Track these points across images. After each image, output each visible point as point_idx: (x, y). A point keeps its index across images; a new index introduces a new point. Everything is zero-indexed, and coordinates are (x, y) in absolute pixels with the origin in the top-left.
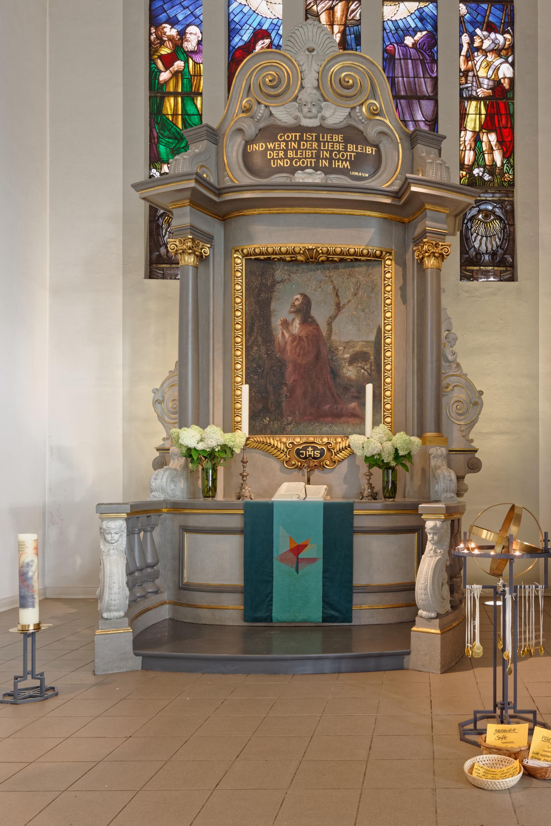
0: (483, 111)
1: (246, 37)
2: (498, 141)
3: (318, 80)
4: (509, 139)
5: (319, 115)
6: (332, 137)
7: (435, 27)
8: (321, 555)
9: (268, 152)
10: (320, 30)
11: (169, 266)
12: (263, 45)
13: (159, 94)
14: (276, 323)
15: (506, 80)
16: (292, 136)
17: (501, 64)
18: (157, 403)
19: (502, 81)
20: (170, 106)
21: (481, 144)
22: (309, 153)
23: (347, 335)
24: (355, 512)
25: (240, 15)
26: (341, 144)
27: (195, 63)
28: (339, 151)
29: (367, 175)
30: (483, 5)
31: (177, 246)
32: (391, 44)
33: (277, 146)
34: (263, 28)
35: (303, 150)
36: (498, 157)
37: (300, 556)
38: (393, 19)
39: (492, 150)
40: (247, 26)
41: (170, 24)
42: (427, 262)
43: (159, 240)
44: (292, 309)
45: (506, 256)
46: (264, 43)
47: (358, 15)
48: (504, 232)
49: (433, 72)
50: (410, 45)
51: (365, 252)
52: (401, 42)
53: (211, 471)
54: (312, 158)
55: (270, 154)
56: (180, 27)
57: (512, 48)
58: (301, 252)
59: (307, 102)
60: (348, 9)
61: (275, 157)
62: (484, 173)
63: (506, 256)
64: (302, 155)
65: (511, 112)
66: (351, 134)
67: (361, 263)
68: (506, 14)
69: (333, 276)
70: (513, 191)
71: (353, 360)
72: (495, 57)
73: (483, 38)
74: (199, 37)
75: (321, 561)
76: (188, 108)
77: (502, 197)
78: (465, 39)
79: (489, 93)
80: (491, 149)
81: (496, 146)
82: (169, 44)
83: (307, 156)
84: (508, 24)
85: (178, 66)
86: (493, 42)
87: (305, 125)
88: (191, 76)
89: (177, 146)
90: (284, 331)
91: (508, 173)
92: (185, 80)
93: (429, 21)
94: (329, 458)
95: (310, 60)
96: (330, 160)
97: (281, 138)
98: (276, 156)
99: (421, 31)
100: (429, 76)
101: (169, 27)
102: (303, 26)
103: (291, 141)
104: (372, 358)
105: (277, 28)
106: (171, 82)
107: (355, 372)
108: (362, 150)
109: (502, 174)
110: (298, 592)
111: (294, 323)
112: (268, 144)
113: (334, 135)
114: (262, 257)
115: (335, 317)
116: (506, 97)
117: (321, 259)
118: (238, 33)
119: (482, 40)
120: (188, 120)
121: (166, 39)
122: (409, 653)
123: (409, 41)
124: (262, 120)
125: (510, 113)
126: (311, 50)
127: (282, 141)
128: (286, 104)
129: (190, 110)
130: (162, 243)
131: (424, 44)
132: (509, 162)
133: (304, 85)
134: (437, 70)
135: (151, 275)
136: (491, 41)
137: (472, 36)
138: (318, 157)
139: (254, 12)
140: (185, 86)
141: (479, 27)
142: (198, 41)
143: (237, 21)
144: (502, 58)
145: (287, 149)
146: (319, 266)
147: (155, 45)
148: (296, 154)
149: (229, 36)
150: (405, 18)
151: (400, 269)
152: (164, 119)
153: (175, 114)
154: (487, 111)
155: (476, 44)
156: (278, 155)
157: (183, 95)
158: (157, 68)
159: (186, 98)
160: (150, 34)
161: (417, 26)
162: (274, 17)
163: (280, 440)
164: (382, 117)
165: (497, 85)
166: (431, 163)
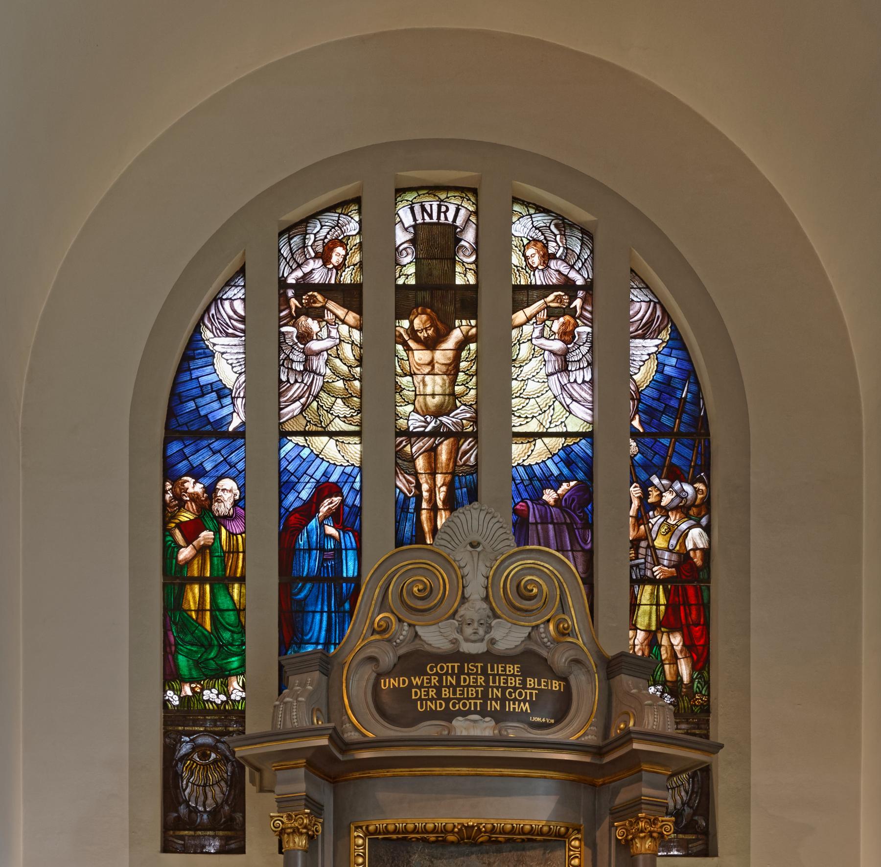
0: (663, 600)
3: (487, 588)
4: (702, 642)
5: (487, 637)
7: (590, 474)
9: (413, 690)
10: (489, 516)
11: (192, 833)
13: (178, 581)
15: (698, 553)
16: (448, 667)
17: (690, 528)
19: (692, 553)
20: (194, 597)
21: (660, 649)
22: (472, 692)
27: (230, 533)
28: (515, 688)
29: (552, 721)
31: (283, 823)
32: (523, 501)
34: (330, 480)
35: (463, 687)
36: (684, 669)
38: (526, 463)
39: (677, 658)
45: (696, 818)
46: (331, 503)
47: (472, 459)
48: (693, 781)
49: (585, 542)
50: (552, 502)
51: (546, 829)
52: (537, 498)
54: (477, 698)
55: (416, 692)
56: (207, 481)
57: (706, 505)
58: (456, 830)
59: (473, 620)
60: (458, 449)
62: (663, 693)
63: (696, 818)
64: (463, 694)
65: (705, 601)
66: (530, 661)
67: (535, 844)
68: (697, 452)
69: (494, 862)
70: (708, 720)
72: (681, 518)
73: (662, 489)
74: (235, 495)
77: (690, 729)
78: (635, 491)
79: (671, 572)
80: (674, 659)
81: (681, 652)
82: (192, 506)
84: (700, 468)
85: (205, 539)
86: (678, 495)
87: (466, 651)
88: (224, 552)
91: (701, 692)
93: (580, 465)
95: (476, 559)
96: (503, 700)
97: (431, 669)
99: (568, 481)
100: (580, 549)
101: (192, 480)
102: (466, 512)
103: (447, 674)
105: (351, 479)
106: (196, 562)
108: (547, 686)
109: (691, 695)
114: (394, 837)
117: (480, 840)
118: (293, 488)
119: (661, 493)
123: (549, 496)
126: (474, 545)
127: (433, 675)
128: (441, 621)
131: (573, 500)
132: (701, 676)
133: (467, 596)
135: (167, 848)
137: (645, 486)
138: (485, 697)
140: (216, 567)
142: (235, 501)
144: (691, 519)
145: (441, 686)
146: (474, 849)
147: (171, 507)
148: (455, 693)
149: (280, 493)
150: (543, 461)
151: (590, 852)
153: (200, 610)
156: (428, 695)
157: (212, 581)
158: (175, 541)
159: (217, 586)
160: (165, 492)
161: (561, 473)
164: (573, 637)
166: (650, 705)
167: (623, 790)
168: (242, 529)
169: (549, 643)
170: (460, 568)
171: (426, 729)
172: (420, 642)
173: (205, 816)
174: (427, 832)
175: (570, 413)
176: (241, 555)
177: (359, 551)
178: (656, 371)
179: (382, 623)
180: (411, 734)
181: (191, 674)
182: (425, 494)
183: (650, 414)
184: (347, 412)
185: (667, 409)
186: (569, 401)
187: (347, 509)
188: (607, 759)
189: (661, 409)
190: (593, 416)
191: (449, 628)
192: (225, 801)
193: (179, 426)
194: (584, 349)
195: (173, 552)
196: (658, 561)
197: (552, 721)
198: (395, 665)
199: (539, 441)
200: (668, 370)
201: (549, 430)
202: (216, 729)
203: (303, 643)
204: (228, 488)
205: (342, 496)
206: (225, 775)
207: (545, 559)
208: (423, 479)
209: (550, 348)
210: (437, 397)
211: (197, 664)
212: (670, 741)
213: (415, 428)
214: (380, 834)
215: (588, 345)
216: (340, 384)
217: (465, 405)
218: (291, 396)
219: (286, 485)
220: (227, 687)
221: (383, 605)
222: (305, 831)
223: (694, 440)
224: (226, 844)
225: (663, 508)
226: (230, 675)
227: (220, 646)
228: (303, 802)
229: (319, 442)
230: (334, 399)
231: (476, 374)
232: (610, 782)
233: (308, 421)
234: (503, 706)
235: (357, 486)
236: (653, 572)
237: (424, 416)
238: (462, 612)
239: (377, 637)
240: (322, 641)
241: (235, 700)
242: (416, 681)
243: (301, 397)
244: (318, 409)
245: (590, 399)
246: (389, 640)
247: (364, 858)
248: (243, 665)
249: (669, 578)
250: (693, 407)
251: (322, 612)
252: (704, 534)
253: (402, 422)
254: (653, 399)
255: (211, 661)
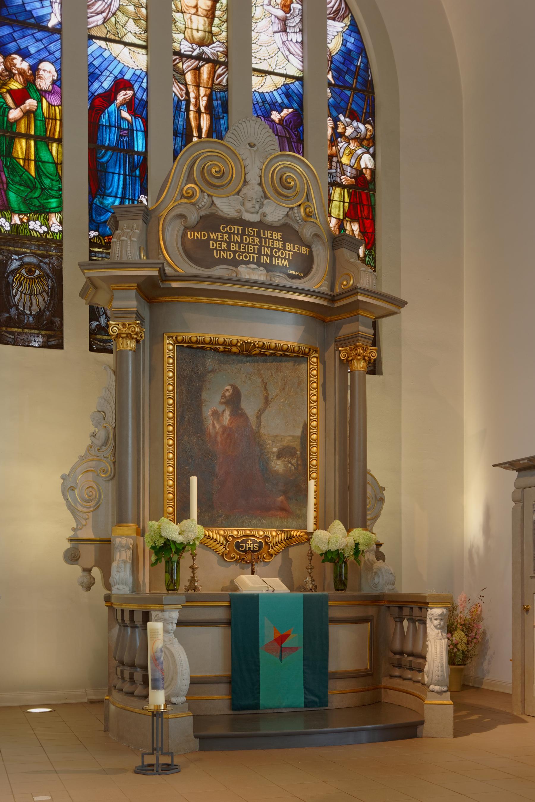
0: (347, 200)
1: (107, 84)
2: (360, 231)
3: (260, 176)
4: (371, 231)
6: (272, 234)
7: (301, 105)
8: (302, 645)
9: (211, 242)
11: (20, 330)
12: (125, 96)
13: (9, 134)
14: (207, 412)
15: (368, 171)
16: (234, 228)
17: (363, 153)
18: (70, 490)
19: (364, 170)
20: (22, 148)
23: (276, 428)
24: (330, 603)
25: (100, 60)
26: (280, 242)
28: (279, 249)
29: (302, 275)
30: (346, 92)
31: (119, 329)
33: (219, 237)
34: (125, 78)
35: (245, 244)
37: (283, 645)
38: (260, 91)
40: (106, 73)
41: (20, 56)
42: (356, 364)
43: (9, 299)
44: (223, 400)
46: (126, 95)
47: (224, 81)
51: (297, 348)
53: (176, 563)
54: (254, 253)
56: (32, 62)
58: (239, 344)
60: (215, 72)
61: (218, 248)
64: (245, 249)
65: (373, 204)
66: (288, 231)
67: (288, 359)
68: (367, 104)
69: (262, 369)
71: (280, 455)
73: (346, 125)
74: (53, 76)
75: (302, 649)
76: (42, 154)
78: (330, 123)
79: (352, 181)
82: (20, 79)
83: (250, 251)
84: (368, 114)
85: (30, 105)
86: (355, 130)
87: (247, 219)
89: (30, 196)
90: (215, 422)
92: (38, 121)
93: (295, 98)
94: (266, 552)
96: (271, 256)
98: (219, 247)
99: (287, 108)
102: (246, 121)
103: (234, 233)
104: (298, 452)
105: (140, 80)
106: (23, 122)
107: (283, 466)
110: (281, 681)
111: (225, 414)
112: (210, 233)
113: (274, 233)
114: (195, 346)
115: (264, 410)
116: (367, 188)
117: (254, 353)
120: (42, 167)
121: (16, 72)
122: (422, 723)
123: (275, 116)
124: (204, 208)
125: (371, 205)
127: (225, 233)
128: (230, 196)
129: (44, 156)
130: (12, 304)
131: (291, 122)
133: (247, 180)
134: (303, 151)
136: (353, 129)
137: (336, 120)
139: (115, 58)
140: (39, 129)
141: (342, 113)
142: (53, 80)
143: (97, 65)
146: (248, 359)
147: (3, 76)
148: (239, 248)
150: (271, 92)
151: (322, 366)
152: (14, 163)
153: (27, 159)
154: (350, 199)
155: (340, 130)
156: (221, 246)
157: (37, 138)
161: (283, 102)
162: (137, 68)
163: (218, 533)
165: (359, 174)
167: (344, 326)
168: (59, 103)
169: (300, 221)
170: (243, 160)
171: (219, 271)
172: (215, 208)
173: (31, 318)
174: (219, 344)
175: (289, 61)
176: (58, 123)
177: (146, 132)
178: (342, 44)
179: (189, 191)
180: (210, 273)
181: (19, 207)
182: (193, 101)
183: (339, 73)
184: (137, 30)
185: (348, 71)
186: (288, 53)
187: (137, 101)
188: (337, 304)
189: (345, 70)
190: (303, 67)
191: (235, 200)
192: (47, 308)
193: (9, 14)
194: (297, 19)
195: (4, 111)
196: (344, 173)
197: (302, 275)
198: (198, 222)
199: (268, 77)
200: (349, 45)
201: (275, 71)
202: (39, 252)
203: (104, 195)
204: (48, 70)
205: (134, 91)
206: (47, 288)
207: (297, 162)
208: (191, 89)
209: (275, 14)
210: (200, 32)
211: (24, 200)
212: (378, 296)
213: (185, 51)
214: (185, 343)
215: (299, 17)
216: (131, 8)
217: (219, 42)
218: (96, 10)
219: (93, 77)
220: (48, 221)
221: (190, 178)
222: (135, 336)
223: (365, 95)
224: (48, 341)
225: (347, 137)
226: (50, 212)
227: (43, 189)
228: (135, 315)
229: (116, 48)
230: (127, 18)
231: (227, 21)
232: (335, 320)
233: (108, 31)
234: (271, 260)
235: (144, 85)
236: (341, 180)
237: (191, 44)
238: (244, 190)
239: (186, 201)
240: (119, 196)
241: (54, 232)
242: (213, 236)
243: (102, 12)
244: (116, 23)
245: (301, 54)
246: (194, 204)
247: (174, 359)
248: (60, 205)
249: (351, 185)
250: (364, 73)
251: (119, 174)
252: (372, 159)
253: (176, 45)
254: (340, 63)
255: (35, 200)
